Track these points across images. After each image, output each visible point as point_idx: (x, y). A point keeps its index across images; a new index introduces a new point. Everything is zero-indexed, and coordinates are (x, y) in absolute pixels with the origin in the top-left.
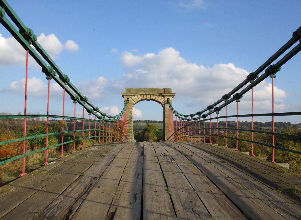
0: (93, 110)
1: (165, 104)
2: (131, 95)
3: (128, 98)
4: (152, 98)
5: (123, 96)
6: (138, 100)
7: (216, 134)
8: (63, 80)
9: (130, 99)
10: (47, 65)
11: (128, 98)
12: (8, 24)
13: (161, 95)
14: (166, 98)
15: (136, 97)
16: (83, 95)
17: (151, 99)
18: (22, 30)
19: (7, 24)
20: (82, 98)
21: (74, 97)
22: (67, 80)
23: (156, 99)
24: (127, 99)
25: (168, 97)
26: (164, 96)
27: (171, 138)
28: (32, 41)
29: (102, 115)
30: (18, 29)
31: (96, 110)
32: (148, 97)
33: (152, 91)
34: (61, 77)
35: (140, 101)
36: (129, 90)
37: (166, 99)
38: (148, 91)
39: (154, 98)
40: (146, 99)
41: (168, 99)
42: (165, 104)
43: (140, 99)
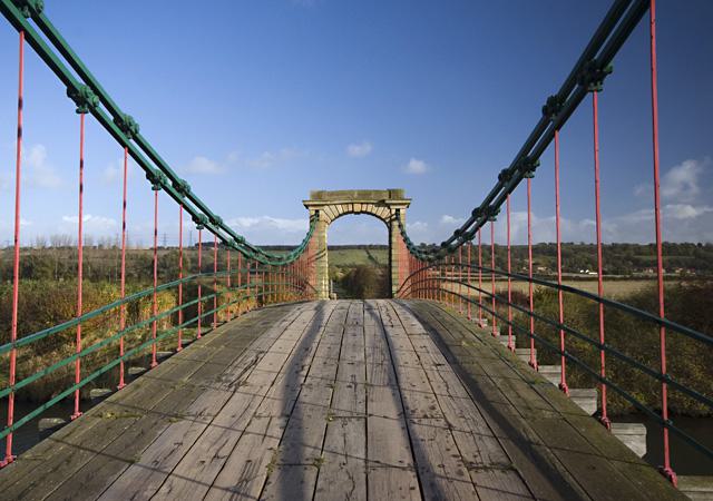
0: (205, 219)
1: (391, 221)
2: (323, 205)
3: (317, 211)
4: (364, 209)
5: (307, 206)
6: (337, 214)
7: (528, 275)
8: (180, 191)
9: (321, 212)
10: (30, 24)
11: (317, 211)
12: (47, 24)
13: (382, 203)
14: (393, 209)
15: (333, 207)
16: (215, 212)
17: (362, 212)
18: (118, 119)
19: (639, 20)
20: (212, 220)
21: (153, 175)
22: (133, 128)
23: (374, 212)
24: (314, 213)
25: (398, 207)
26: (388, 206)
27: (405, 287)
28: (132, 133)
29: (236, 239)
30: (112, 118)
31: (216, 222)
32: (357, 208)
33: (365, 196)
34: (176, 184)
35: (340, 215)
36: (318, 196)
37: (393, 212)
38: (356, 196)
39: (369, 210)
40: (352, 212)
41: (398, 210)
42: (391, 221)
43: (341, 212)
